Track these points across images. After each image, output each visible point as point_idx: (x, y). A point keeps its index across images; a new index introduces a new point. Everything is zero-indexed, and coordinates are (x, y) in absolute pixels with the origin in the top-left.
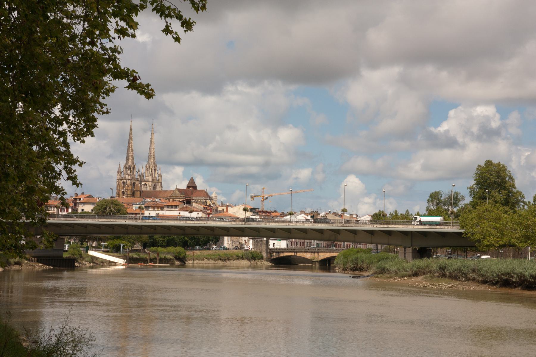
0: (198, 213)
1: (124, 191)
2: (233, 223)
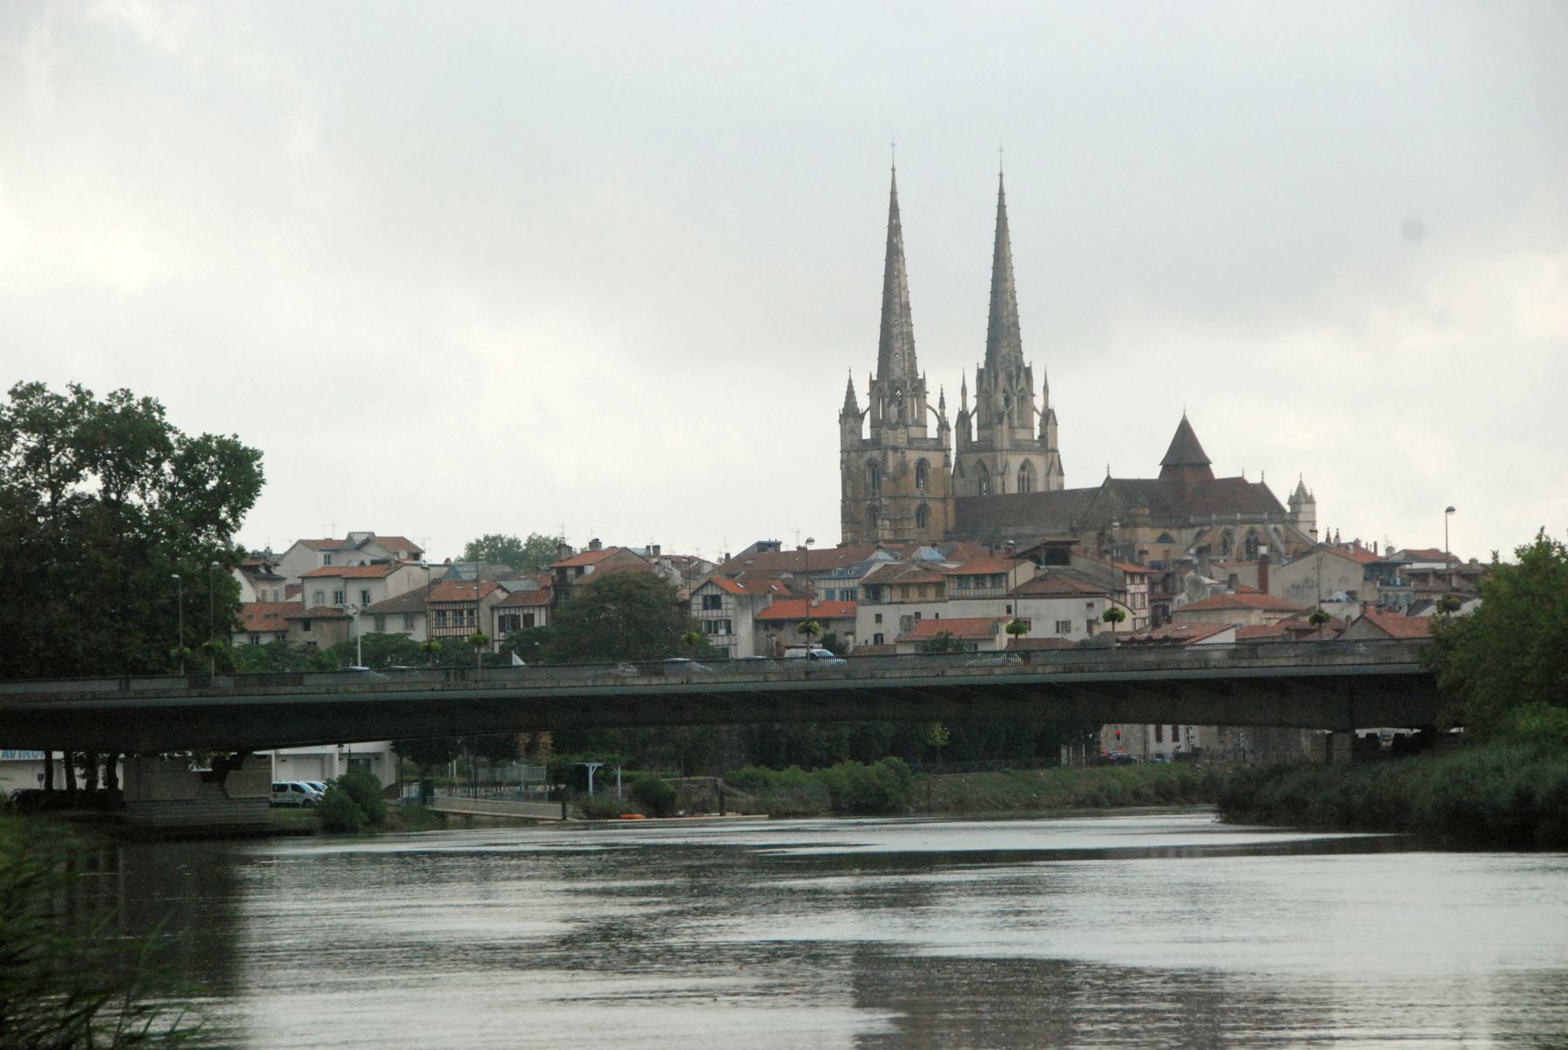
0: (1090, 605)
1: (877, 503)
2: (655, 681)
